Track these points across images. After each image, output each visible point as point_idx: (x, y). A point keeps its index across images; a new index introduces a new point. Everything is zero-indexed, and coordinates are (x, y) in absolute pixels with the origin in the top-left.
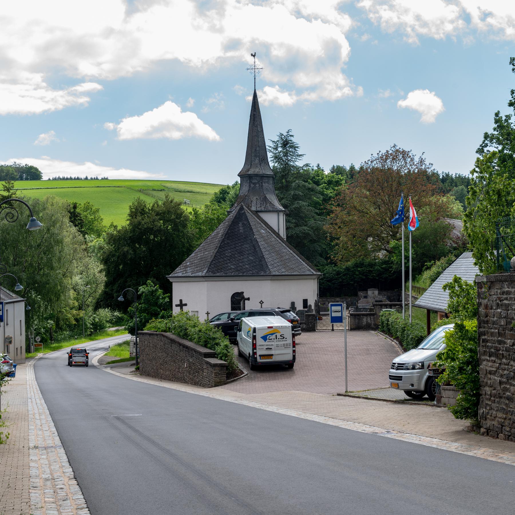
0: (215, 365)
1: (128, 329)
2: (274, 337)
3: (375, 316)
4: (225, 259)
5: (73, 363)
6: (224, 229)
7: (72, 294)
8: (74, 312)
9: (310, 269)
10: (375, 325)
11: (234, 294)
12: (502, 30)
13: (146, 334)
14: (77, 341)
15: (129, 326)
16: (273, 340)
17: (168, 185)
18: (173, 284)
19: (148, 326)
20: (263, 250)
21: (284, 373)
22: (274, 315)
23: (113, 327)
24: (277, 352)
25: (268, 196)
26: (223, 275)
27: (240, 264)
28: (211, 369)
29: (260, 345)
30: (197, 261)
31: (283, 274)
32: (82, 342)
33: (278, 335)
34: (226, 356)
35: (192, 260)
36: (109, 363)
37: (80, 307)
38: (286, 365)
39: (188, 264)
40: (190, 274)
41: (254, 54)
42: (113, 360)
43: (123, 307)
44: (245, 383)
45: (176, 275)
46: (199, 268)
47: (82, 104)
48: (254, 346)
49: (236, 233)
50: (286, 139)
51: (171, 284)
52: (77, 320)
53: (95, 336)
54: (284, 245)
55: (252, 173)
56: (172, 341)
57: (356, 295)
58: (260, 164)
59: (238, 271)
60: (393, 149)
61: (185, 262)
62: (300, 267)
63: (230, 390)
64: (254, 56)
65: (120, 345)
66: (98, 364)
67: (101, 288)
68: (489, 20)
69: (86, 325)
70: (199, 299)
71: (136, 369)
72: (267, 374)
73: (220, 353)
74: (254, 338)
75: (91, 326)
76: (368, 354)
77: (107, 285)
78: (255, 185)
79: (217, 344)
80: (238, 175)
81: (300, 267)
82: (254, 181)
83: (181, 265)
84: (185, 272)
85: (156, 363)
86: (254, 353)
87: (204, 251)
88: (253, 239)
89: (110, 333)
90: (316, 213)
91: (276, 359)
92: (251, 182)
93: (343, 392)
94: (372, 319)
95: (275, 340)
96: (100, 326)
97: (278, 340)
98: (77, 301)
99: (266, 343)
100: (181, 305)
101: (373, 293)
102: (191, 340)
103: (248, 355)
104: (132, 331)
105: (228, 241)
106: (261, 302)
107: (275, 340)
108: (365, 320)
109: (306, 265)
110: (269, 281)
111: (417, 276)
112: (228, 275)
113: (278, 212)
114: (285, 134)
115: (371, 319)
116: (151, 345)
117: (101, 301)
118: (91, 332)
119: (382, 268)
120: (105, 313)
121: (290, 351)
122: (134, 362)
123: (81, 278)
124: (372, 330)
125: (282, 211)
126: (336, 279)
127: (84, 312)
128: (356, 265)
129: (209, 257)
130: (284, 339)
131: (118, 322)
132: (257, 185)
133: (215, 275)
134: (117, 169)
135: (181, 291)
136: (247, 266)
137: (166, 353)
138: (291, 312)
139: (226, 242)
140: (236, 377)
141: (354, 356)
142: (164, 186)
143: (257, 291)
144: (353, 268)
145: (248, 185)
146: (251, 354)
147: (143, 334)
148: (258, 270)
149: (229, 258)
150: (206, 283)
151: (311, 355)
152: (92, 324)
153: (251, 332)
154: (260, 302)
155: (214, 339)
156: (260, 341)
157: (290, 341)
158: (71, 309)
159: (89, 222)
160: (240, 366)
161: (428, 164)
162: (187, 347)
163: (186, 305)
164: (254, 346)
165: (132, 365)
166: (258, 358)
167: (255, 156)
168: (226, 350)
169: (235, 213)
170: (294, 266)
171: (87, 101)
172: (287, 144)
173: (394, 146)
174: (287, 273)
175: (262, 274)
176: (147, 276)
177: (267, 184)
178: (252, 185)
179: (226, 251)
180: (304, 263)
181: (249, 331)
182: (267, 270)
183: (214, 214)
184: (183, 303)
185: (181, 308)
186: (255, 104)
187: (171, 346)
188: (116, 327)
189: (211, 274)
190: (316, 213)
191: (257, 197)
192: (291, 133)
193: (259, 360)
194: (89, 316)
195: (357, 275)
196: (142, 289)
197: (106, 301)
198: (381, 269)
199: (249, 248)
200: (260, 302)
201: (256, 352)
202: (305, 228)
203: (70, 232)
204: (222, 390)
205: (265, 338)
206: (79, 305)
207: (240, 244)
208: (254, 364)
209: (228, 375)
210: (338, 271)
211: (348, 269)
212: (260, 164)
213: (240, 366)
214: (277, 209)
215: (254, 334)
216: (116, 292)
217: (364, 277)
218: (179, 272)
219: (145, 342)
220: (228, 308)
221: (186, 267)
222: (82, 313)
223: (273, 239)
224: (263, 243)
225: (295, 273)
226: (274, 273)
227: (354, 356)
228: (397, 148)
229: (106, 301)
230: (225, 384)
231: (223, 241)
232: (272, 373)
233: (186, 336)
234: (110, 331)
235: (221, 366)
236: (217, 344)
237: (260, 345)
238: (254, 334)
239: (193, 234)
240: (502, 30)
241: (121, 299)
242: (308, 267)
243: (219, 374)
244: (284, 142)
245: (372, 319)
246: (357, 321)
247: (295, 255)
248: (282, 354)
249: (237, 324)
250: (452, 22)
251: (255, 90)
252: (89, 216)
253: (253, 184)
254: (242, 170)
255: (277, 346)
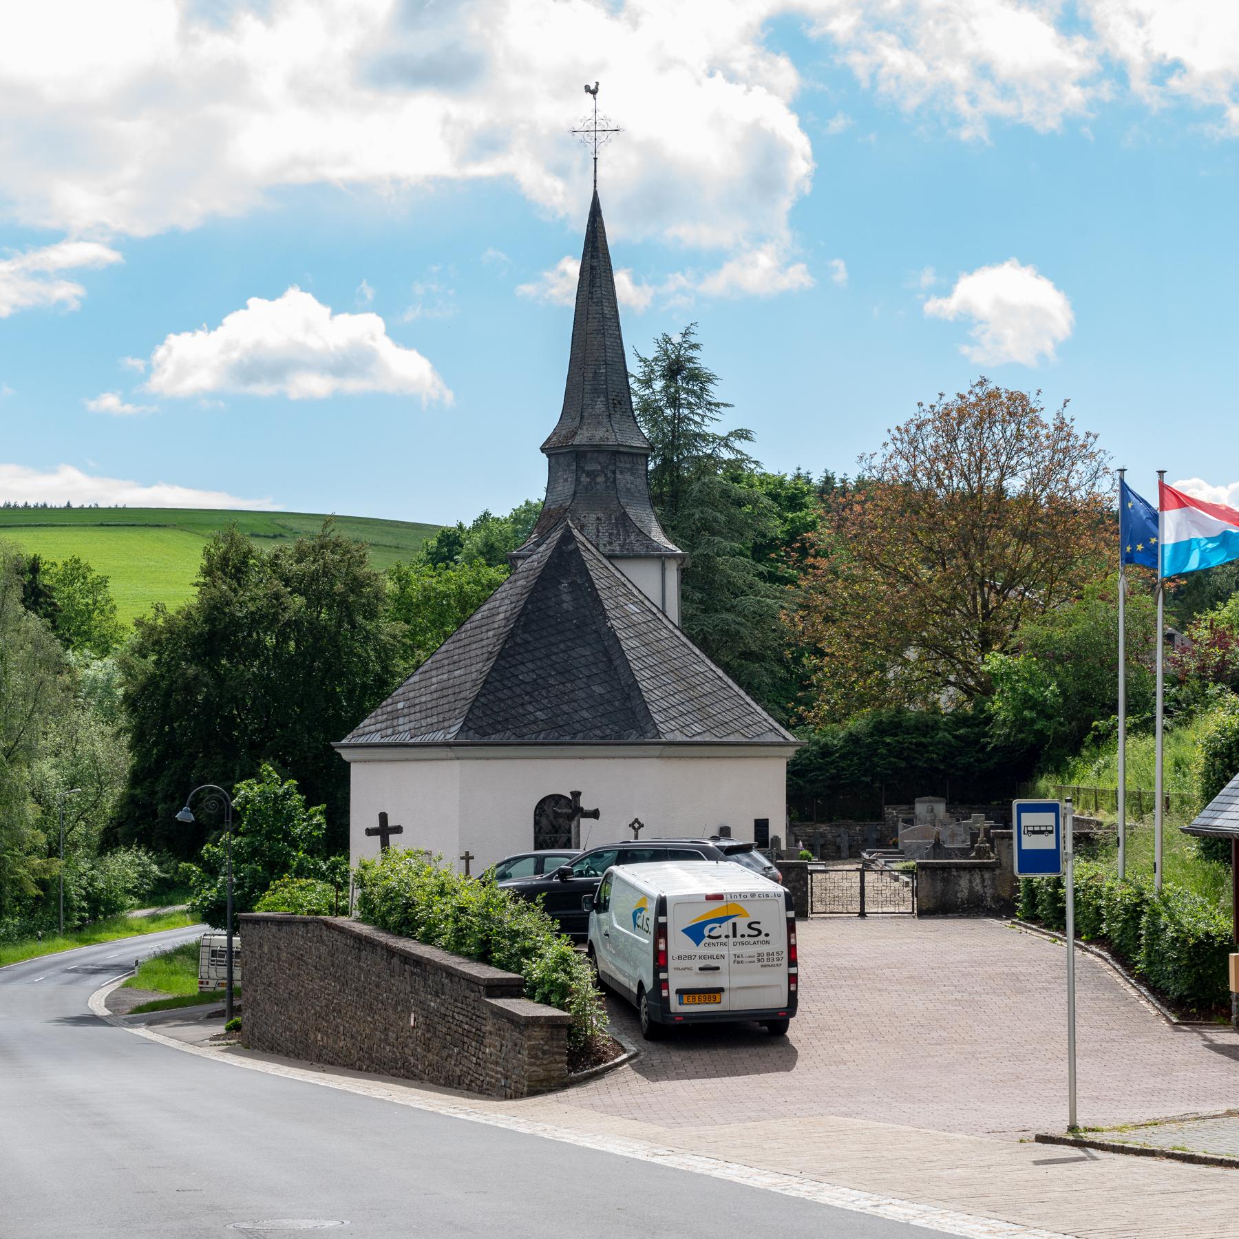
0: (534, 1021)
1: (193, 910)
2: (726, 928)
3: (998, 872)
4: (518, 690)
5: (565, 1033)
6: (514, 599)
7: (32, 811)
8: (37, 862)
9: (777, 725)
10: (997, 899)
11: (543, 801)
12: (1216, 113)
13: (266, 920)
14: (43, 945)
15: (205, 899)
16: (723, 940)
17: (293, 524)
18: (353, 766)
19: (268, 898)
20: (635, 665)
21: (761, 1050)
22: (701, 858)
23: (140, 908)
24: (737, 981)
25: (632, 512)
26: (513, 739)
27: (565, 708)
28: (512, 1035)
29: (680, 958)
30: (428, 698)
31: (698, 739)
32: (58, 949)
33: (742, 928)
34: (564, 990)
35: (412, 695)
36: (139, 1009)
37: (50, 848)
38: (762, 1023)
39: (400, 705)
40: (406, 738)
41: (592, 87)
42: (152, 999)
43: (185, 843)
44: (634, 1086)
45: (361, 740)
46: (435, 719)
47: (62, 304)
48: (661, 961)
49: (551, 613)
50: (678, 356)
51: (347, 766)
52: (42, 884)
53: (94, 932)
54: (697, 651)
55: (584, 442)
56: (360, 939)
57: (878, 816)
58: (609, 416)
59: (557, 727)
60: (977, 390)
61: (390, 701)
62: (748, 720)
63: (593, 1107)
64: (594, 92)
65: (167, 957)
66: (106, 1012)
67: (116, 792)
68: (1174, 82)
69: (67, 899)
70: (434, 816)
71: (229, 1029)
72: (704, 1057)
73: (542, 982)
74: (661, 931)
75: (84, 904)
76: (1020, 992)
77: (137, 778)
78: (594, 479)
79: (527, 953)
80: (543, 450)
81: (748, 720)
82: (590, 467)
83: (379, 711)
84: (389, 731)
85: (301, 1012)
86: (660, 984)
87: (452, 669)
88: (604, 630)
89: (135, 924)
90: (760, 575)
91: (731, 1002)
92: (580, 469)
93: (1060, 1130)
94: (988, 882)
95: (731, 939)
96: (108, 903)
97: (739, 939)
98: (45, 830)
99: (702, 950)
100: (384, 831)
101: (932, 810)
102: (428, 940)
103: (635, 990)
104: (213, 915)
105: (526, 636)
106: (636, 825)
107: (731, 939)
108: (964, 883)
109: (765, 715)
110: (656, 762)
111: (1069, 759)
112: (526, 740)
113: (664, 558)
114: (677, 339)
115: (983, 881)
116: (284, 956)
117: (120, 825)
118: (82, 919)
119: (955, 737)
120: (127, 865)
121: (779, 976)
122: (221, 1005)
123: (55, 766)
124: (988, 916)
125: (674, 556)
126: (819, 769)
127: (62, 862)
128: (879, 729)
129: (468, 685)
130: (762, 938)
131: (160, 893)
132: (600, 479)
133: (485, 740)
134: (148, 485)
135: (373, 789)
136: (585, 714)
137: (337, 979)
138: (755, 854)
139: (518, 640)
140: (600, 1061)
141: (977, 998)
142: (283, 527)
143: (619, 790)
144: (872, 735)
145: (572, 478)
146: (649, 985)
147: (257, 921)
148: (622, 722)
149: (529, 689)
150: (457, 762)
151: (831, 992)
152: (87, 897)
153: (652, 907)
154: (632, 825)
155: (514, 935)
156: (678, 944)
157: (779, 944)
158: (28, 854)
159: (79, 613)
160: (601, 1024)
161: (1082, 437)
162: (419, 962)
163: (398, 830)
164: (661, 961)
165: (213, 1017)
166: (674, 999)
167: (595, 391)
168: (565, 971)
169: (549, 553)
170: (728, 717)
171: (76, 297)
172: (678, 371)
173: (983, 382)
174: (707, 738)
175: (632, 739)
176: (257, 752)
177: (628, 477)
178: (585, 479)
179: (522, 668)
180: (759, 709)
181: (641, 910)
182: (649, 727)
183: (449, 580)
184: (391, 823)
185: (385, 843)
186: (594, 242)
187: (358, 959)
188: (149, 907)
189: (473, 737)
190: (760, 575)
191: (601, 515)
192: (693, 339)
193: (675, 1006)
194: (79, 872)
195: (882, 757)
196: (246, 790)
197: (137, 824)
198: (953, 740)
199: (591, 659)
200: (632, 825)
201: (666, 981)
202: (730, 616)
203: (27, 632)
204: (564, 1107)
205: (695, 933)
206: (49, 843)
207: (562, 646)
208: (658, 1020)
209: (569, 1060)
210: (826, 745)
211: (853, 738)
212: (609, 416)
213: (601, 1024)
214: (658, 549)
215: (662, 919)
216: (164, 800)
217: (903, 764)
218: (371, 728)
219: (261, 946)
220: (523, 841)
221: (394, 715)
222: (57, 866)
223: (665, 633)
224: (633, 643)
225: (731, 739)
226: (670, 737)
227: (977, 998)
228: (991, 387)
229: (137, 824)
230: (564, 1085)
231: (511, 635)
232: (722, 1052)
233: (406, 925)
234: (136, 918)
235: (551, 1022)
236: (527, 953)
237: (680, 958)
238: (662, 919)
239: (394, 637)
240: (1216, 113)
241: (184, 815)
242: (771, 720)
243: (544, 1052)
244: (670, 365)
245: (988, 882)
246: (939, 886)
247: (730, 682)
248: (748, 987)
249: (591, 888)
250: (1082, 83)
251: (595, 193)
252: (78, 595)
253: (588, 474)
254: (554, 433)
255: (738, 960)
